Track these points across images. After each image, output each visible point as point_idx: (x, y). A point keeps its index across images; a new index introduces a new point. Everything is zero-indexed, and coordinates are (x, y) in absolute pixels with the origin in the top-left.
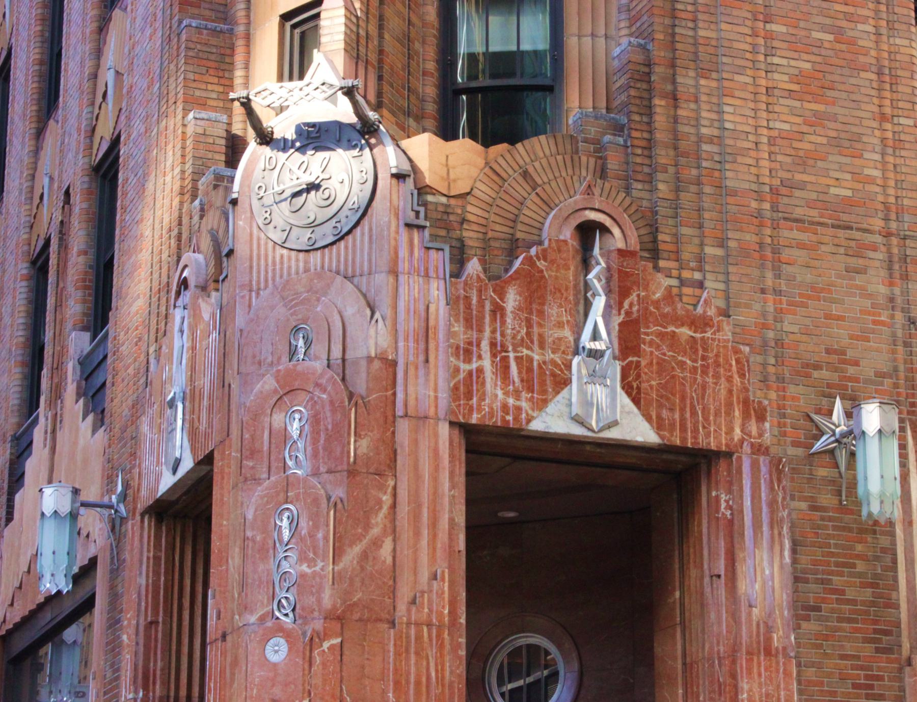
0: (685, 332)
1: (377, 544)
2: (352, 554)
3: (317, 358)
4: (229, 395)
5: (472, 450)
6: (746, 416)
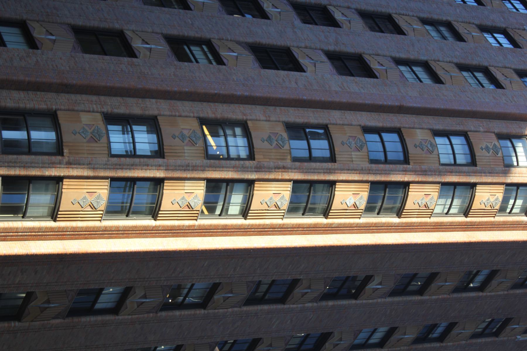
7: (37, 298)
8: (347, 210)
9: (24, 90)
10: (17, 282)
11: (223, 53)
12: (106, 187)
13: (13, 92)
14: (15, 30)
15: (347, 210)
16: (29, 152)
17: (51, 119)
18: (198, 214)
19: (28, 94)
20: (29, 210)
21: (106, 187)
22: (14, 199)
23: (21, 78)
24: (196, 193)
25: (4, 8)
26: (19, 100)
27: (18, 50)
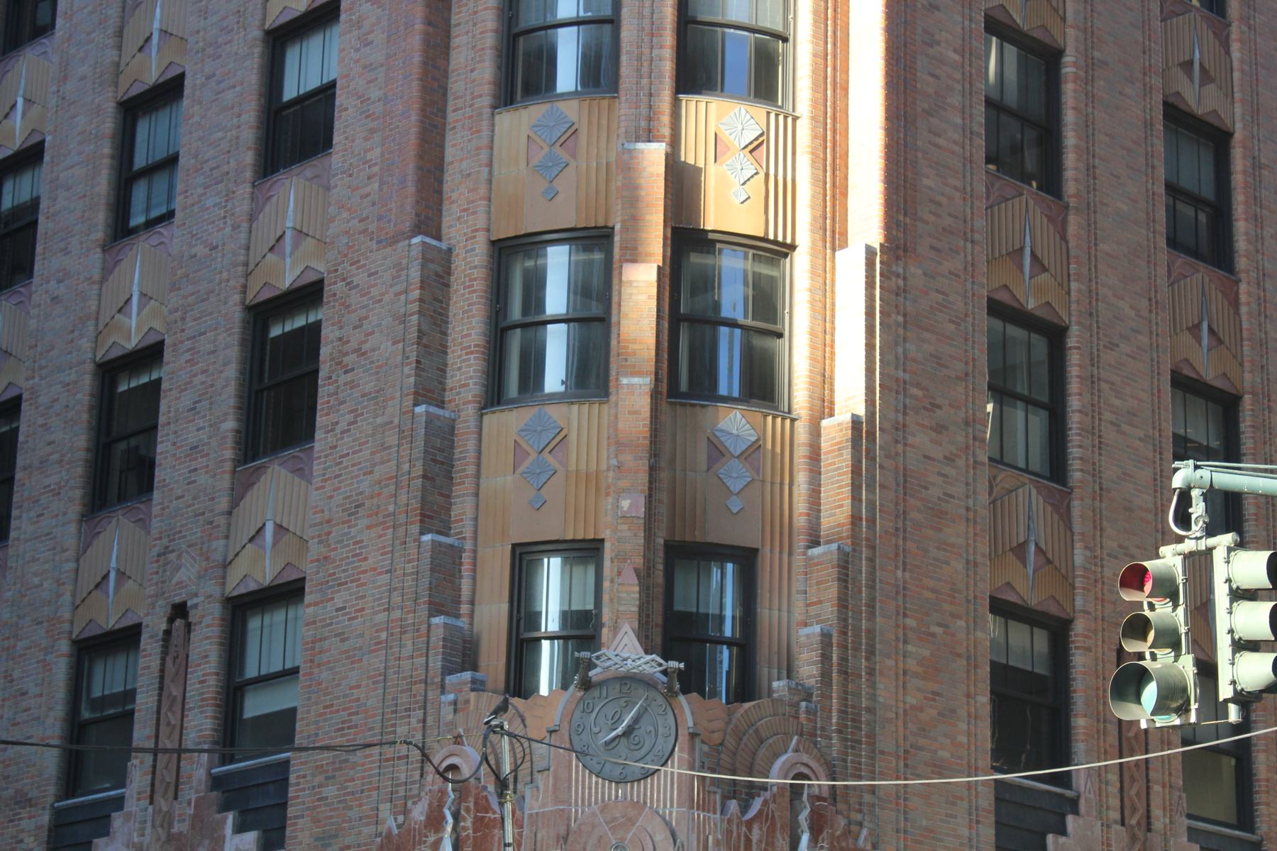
7: (1002, 5)
8: (767, 175)
9: (447, 36)
10: (957, 57)
12: (702, 106)
13: (453, 64)
14: (292, 56)
15: (767, 175)
16: (613, 22)
17: (512, 252)
18: (777, 115)
19: (459, 24)
21: (702, 106)
22: (737, 57)
23: (416, 40)
24: (719, 126)
25: (234, 87)
26: (474, 47)
27: (341, 51)
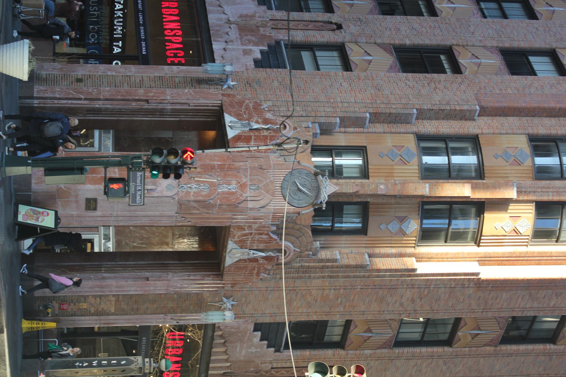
0: (256, 272)
1: (198, 210)
2: (195, 205)
3: (250, 192)
4: (400, 133)
5: (226, 227)
6: (232, 284)
10: (552, 305)
11: (462, 61)
14: (546, 59)
15: (505, 236)
17: (474, 143)
20: (562, 234)
21: (531, 211)
22: (550, 224)
24: (524, 218)
